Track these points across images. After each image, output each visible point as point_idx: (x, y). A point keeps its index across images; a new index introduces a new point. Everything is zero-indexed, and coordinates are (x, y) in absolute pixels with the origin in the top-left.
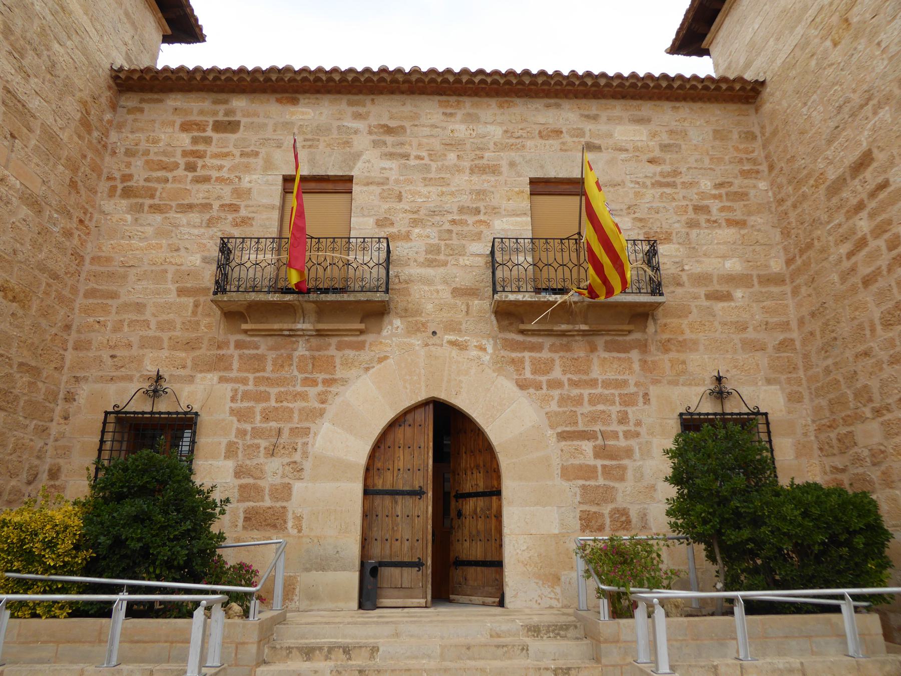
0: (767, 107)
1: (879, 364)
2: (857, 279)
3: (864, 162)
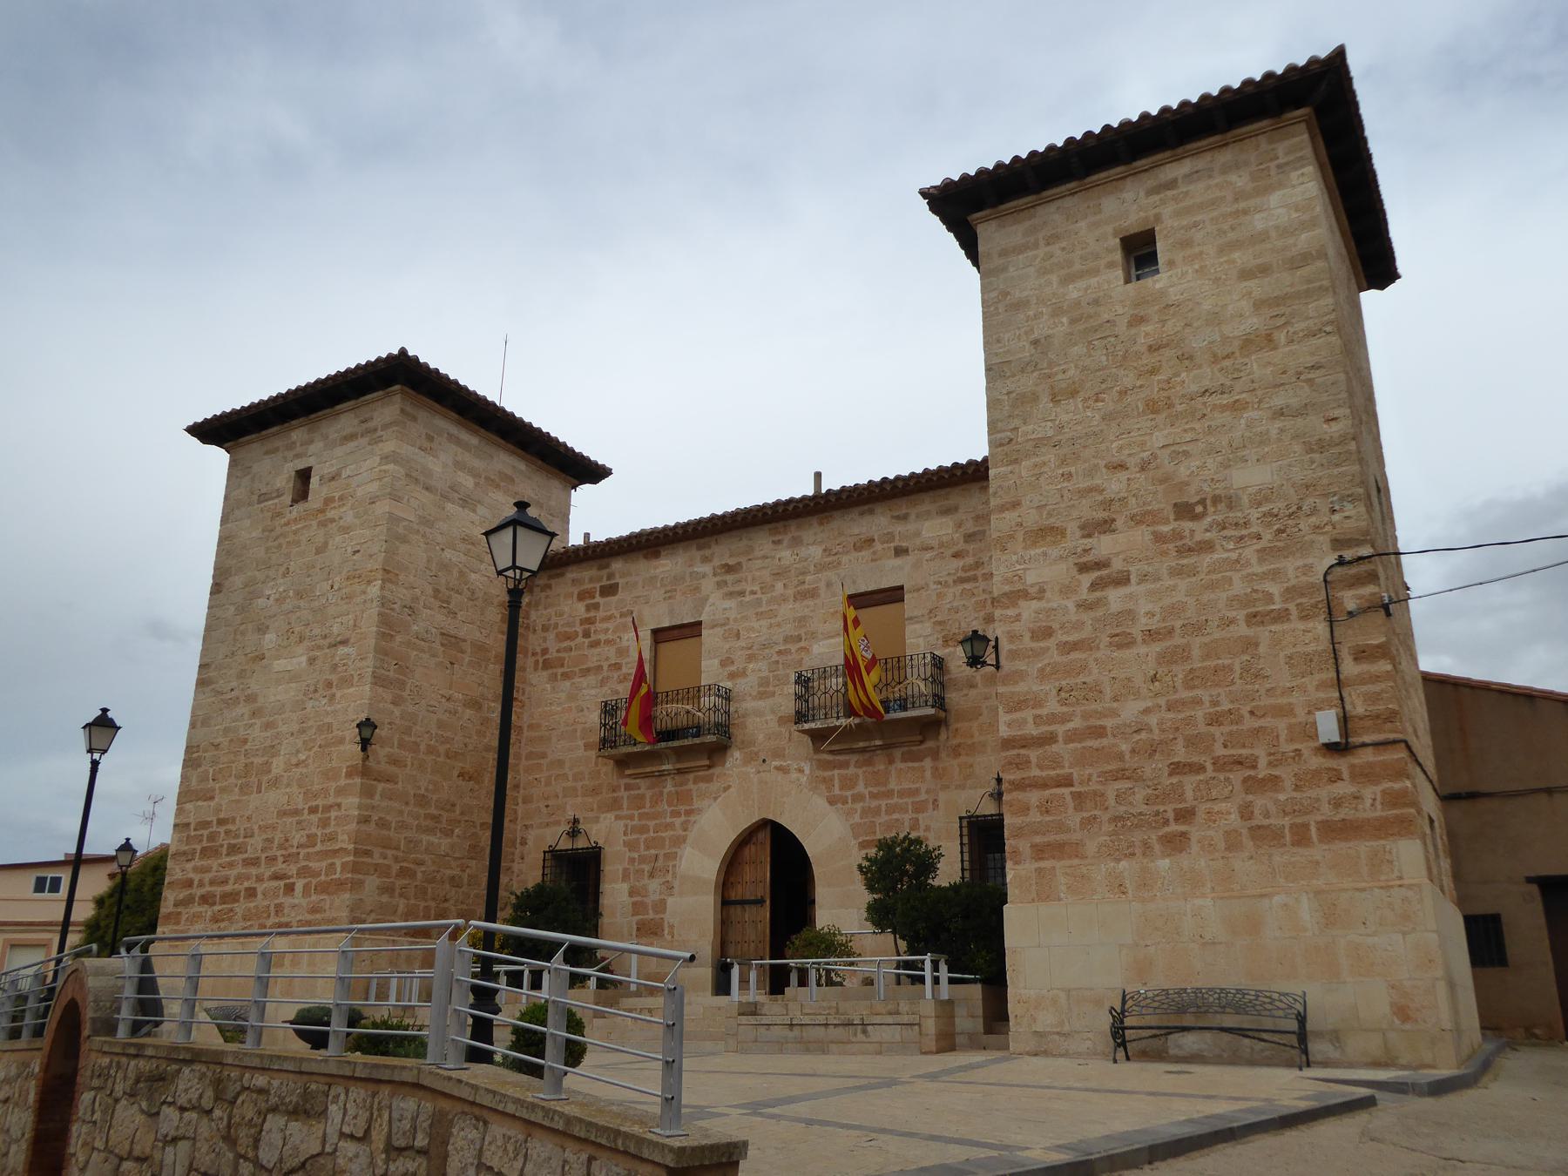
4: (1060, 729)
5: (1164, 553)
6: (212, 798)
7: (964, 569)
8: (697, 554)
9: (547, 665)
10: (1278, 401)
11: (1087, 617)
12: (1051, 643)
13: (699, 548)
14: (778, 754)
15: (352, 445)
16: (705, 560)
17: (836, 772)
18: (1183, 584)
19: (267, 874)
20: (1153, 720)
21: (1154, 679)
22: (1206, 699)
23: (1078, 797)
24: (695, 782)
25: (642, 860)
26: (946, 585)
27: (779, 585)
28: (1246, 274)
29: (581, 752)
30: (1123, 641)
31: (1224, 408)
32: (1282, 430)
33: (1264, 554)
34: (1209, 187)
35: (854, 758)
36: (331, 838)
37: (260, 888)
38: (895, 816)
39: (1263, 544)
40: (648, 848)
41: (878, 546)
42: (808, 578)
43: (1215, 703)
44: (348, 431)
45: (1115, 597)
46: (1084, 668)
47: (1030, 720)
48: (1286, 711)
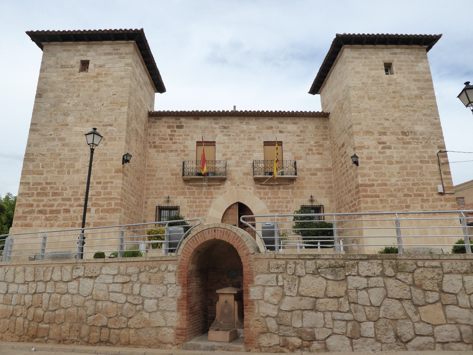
4: (375, 183)
5: (400, 143)
6: (42, 174)
7: (300, 140)
8: (214, 121)
9: (155, 147)
10: (424, 112)
11: (381, 156)
12: (371, 161)
13: (214, 120)
14: (243, 183)
15: (110, 57)
16: (216, 123)
17: (262, 190)
18: (405, 151)
19: (75, 204)
20: (399, 183)
21: (399, 173)
22: (411, 179)
23: (380, 200)
24: (214, 189)
25: (194, 211)
26: (295, 143)
27: (242, 135)
28: (415, 80)
29: (170, 176)
30: (391, 163)
31: (412, 111)
32: (425, 119)
33: (423, 147)
34: (405, 57)
35: (267, 187)
36: (109, 193)
37: (72, 209)
38: (281, 204)
39: (422, 145)
40: (196, 207)
41: (274, 129)
42: (252, 135)
43: (414, 181)
44: (108, 51)
45: (388, 152)
46: (381, 168)
47: (367, 180)
48: (429, 184)
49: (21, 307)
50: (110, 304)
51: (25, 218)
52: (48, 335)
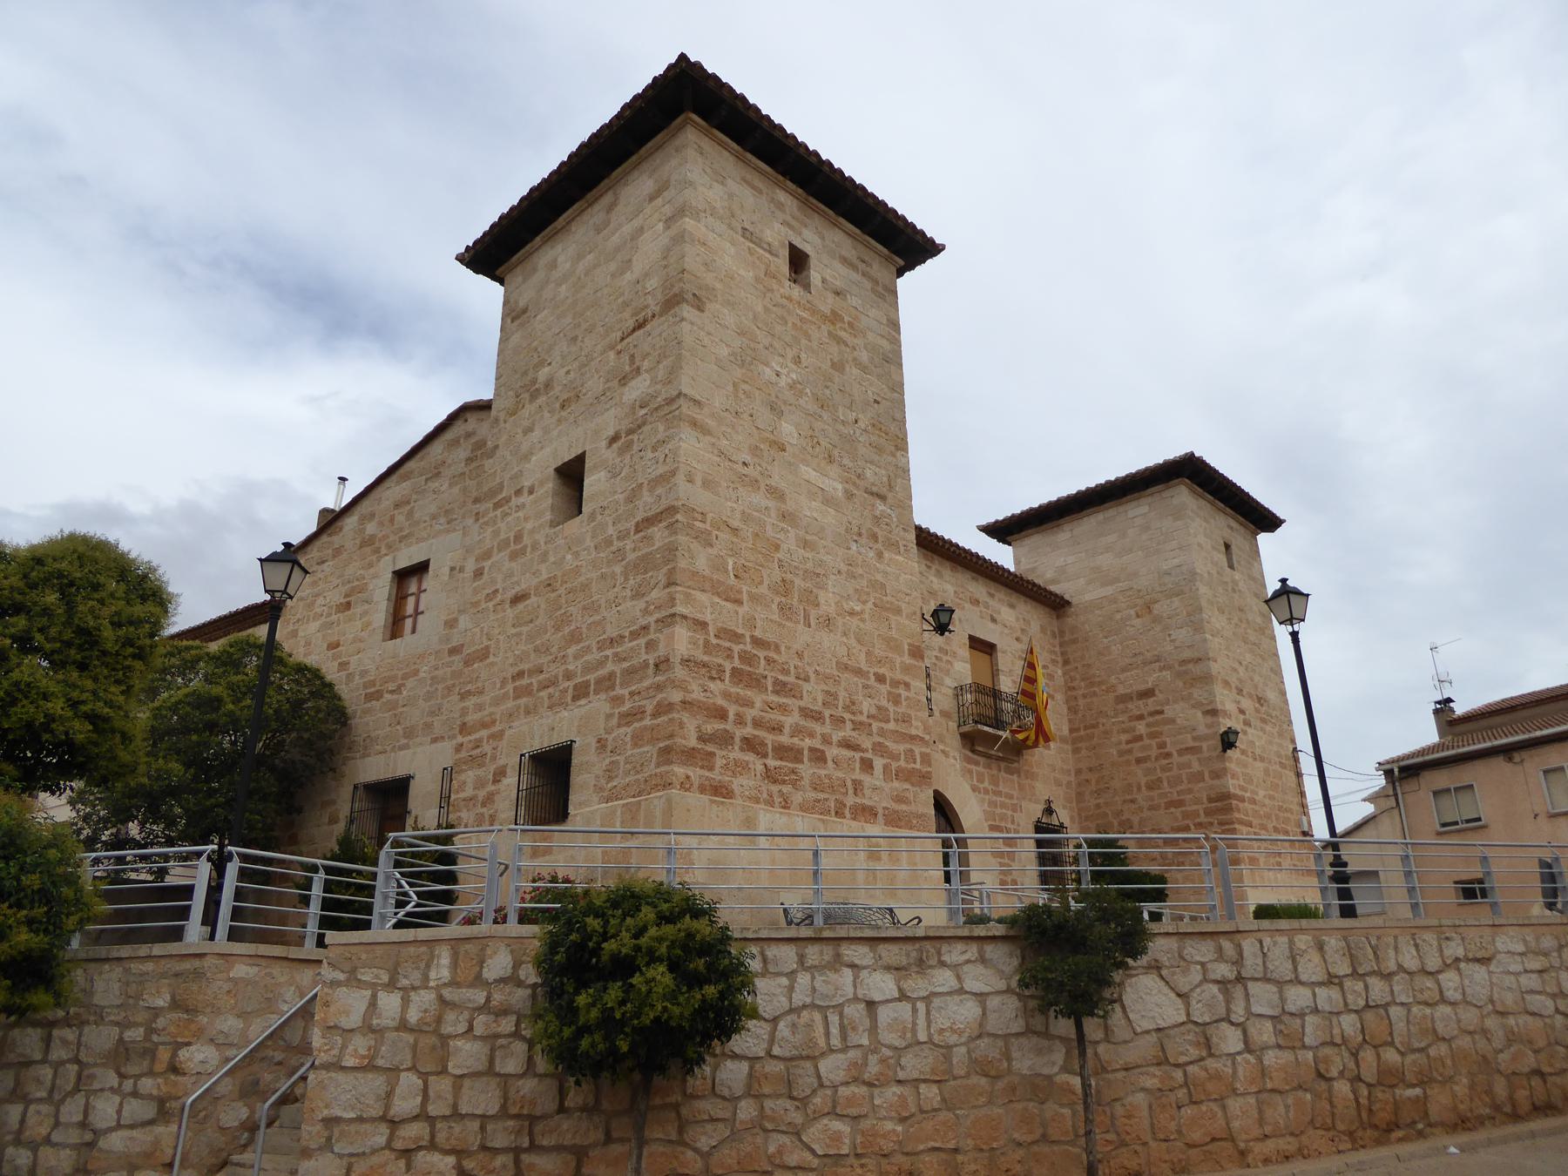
0: (1070, 621)
1: (1141, 809)
2: (1131, 758)
3: (1147, 694)
49: (1336, 1050)
50: (1530, 1019)
51: (707, 760)
52: (1426, 1114)
